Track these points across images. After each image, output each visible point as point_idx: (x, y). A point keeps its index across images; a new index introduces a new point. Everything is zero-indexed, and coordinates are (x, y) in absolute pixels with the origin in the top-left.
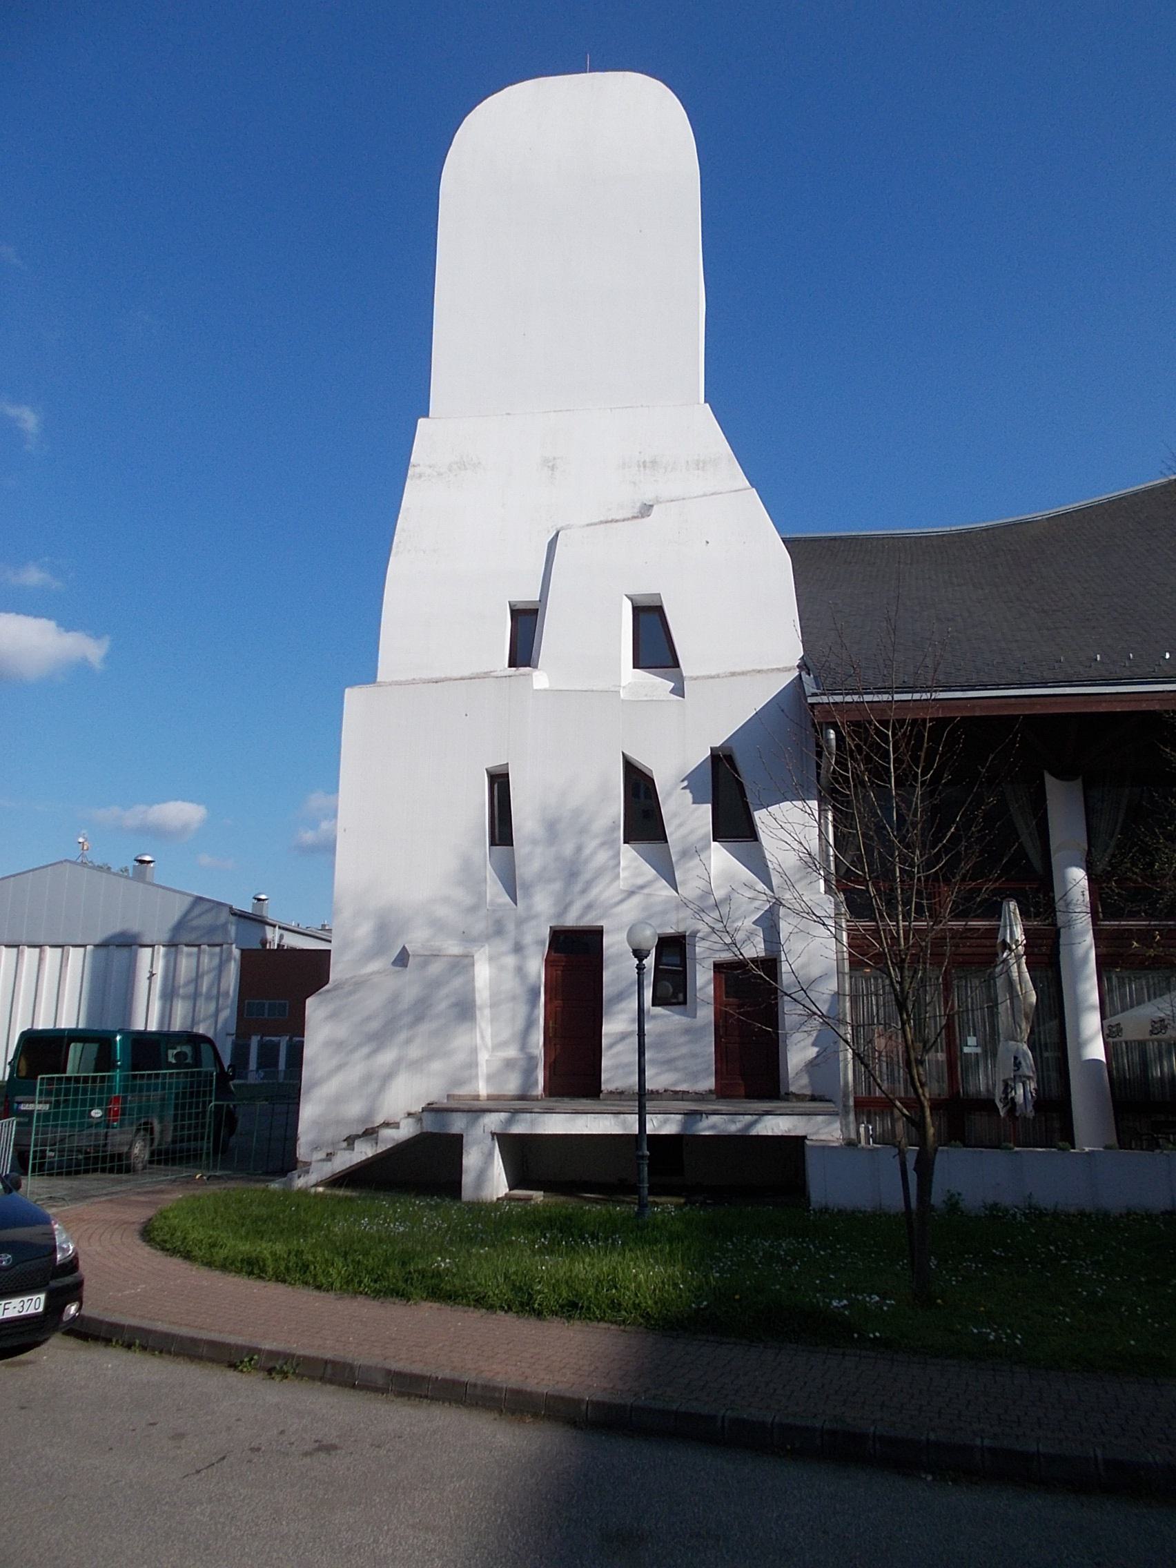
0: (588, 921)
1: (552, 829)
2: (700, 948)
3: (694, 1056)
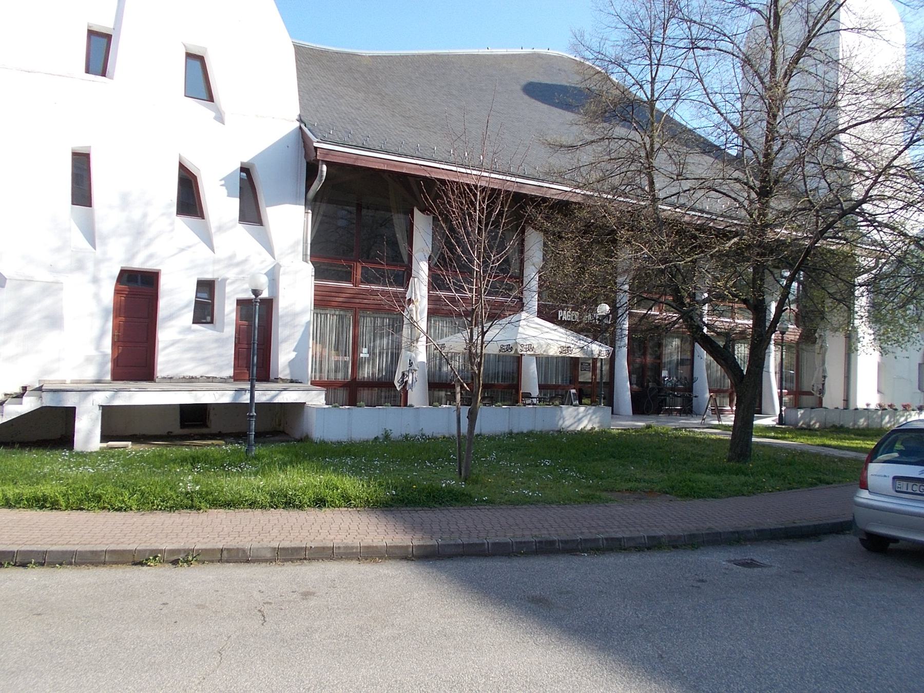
0: (149, 266)
1: (125, 201)
2: (228, 289)
3: (220, 355)
